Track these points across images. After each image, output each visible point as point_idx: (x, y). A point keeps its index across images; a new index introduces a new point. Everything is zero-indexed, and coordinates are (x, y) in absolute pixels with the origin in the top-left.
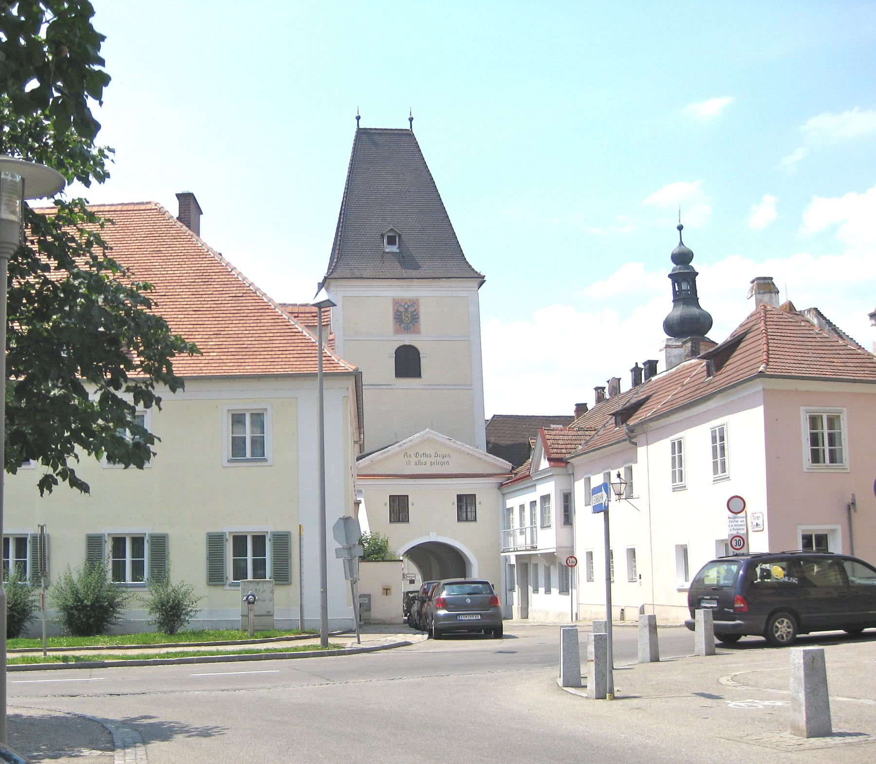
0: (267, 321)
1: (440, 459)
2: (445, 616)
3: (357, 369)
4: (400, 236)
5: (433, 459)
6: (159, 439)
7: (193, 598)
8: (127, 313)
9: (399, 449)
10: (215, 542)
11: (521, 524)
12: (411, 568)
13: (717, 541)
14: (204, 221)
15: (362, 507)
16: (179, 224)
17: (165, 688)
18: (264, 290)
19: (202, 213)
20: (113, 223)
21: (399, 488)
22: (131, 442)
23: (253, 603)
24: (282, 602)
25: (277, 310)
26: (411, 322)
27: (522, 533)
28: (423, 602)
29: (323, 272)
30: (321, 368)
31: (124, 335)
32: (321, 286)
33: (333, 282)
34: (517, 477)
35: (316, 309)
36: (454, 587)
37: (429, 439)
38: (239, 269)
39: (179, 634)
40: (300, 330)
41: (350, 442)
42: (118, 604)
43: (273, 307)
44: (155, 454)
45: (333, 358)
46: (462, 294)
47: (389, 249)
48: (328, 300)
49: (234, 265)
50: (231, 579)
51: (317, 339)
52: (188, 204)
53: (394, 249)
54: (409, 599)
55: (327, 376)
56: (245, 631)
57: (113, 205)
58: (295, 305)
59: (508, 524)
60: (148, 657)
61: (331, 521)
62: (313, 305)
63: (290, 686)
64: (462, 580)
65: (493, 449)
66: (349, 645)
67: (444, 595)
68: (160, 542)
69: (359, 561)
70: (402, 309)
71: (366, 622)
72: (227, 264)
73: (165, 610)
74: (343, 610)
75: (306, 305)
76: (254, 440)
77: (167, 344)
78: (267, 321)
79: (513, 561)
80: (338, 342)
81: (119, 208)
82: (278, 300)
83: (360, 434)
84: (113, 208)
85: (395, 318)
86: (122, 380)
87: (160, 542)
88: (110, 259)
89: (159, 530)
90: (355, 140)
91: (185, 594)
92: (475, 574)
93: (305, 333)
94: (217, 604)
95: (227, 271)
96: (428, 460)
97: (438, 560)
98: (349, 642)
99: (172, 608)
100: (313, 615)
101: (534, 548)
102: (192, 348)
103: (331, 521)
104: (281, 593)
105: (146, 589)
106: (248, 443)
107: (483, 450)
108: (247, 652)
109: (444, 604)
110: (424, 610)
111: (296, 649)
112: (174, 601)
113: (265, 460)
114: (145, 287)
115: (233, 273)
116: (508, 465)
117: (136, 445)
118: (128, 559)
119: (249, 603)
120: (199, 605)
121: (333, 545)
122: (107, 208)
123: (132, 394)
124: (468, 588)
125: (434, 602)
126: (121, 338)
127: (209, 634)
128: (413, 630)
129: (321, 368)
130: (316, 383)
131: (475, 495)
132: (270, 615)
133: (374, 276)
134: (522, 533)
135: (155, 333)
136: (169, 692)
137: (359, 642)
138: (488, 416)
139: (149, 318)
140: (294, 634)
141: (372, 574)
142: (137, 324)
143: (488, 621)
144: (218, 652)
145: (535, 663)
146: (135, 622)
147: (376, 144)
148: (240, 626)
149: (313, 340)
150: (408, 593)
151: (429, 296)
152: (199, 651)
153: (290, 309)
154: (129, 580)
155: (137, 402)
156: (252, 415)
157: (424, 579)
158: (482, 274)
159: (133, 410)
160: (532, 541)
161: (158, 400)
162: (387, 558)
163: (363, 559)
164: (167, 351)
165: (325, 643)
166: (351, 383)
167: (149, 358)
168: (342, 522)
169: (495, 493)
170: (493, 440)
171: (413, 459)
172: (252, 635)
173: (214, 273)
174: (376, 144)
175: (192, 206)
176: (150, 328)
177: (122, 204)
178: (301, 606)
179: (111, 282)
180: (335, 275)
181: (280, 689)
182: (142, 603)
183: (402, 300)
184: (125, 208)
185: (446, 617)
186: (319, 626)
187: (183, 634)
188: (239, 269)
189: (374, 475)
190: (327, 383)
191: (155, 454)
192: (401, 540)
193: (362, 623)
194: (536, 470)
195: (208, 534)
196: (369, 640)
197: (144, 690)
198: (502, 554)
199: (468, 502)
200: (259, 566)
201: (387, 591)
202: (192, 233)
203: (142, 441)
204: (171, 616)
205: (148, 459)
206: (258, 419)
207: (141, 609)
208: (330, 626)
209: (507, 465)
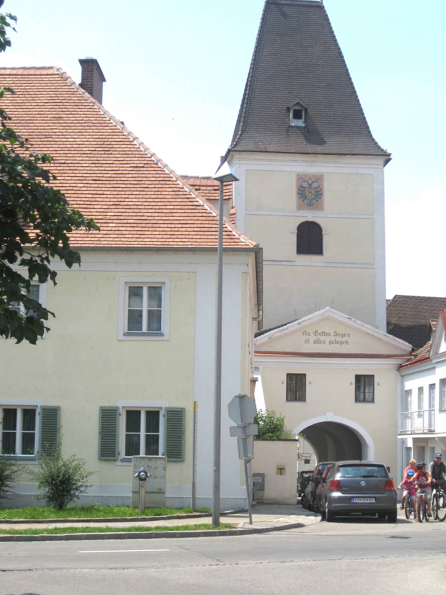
0: (168, 192)
1: (339, 339)
2: (340, 498)
3: (257, 246)
4: (306, 110)
5: (332, 338)
6: (53, 314)
7: (84, 473)
8: (25, 186)
9: (298, 327)
10: (108, 416)
11: (420, 407)
12: (306, 447)
13: (357, 400)
14: (107, 88)
15: (259, 385)
16: (82, 90)
17: (52, 565)
18: (165, 161)
19: (104, 80)
20: (13, 93)
21: (297, 366)
22: (25, 316)
23: (145, 479)
24: (175, 480)
25: (178, 182)
26: (314, 198)
27: (420, 416)
28: (317, 483)
29: (226, 142)
30: (221, 242)
31: (21, 207)
32: (224, 159)
33: (237, 156)
34: (417, 358)
35: (217, 183)
36: (349, 469)
37: (328, 318)
38: (141, 139)
39: (69, 509)
40: (201, 203)
41: (248, 319)
42: (8, 477)
43: (174, 179)
44: (48, 329)
45: (234, 233)
46: (367, 171)
47: (295, 123)
48: (231, 175)
49: (136, 134)
50: (123, 455)
51: (218, 212)
52: (92, 72)
53: (300, 123)
54: (304, 480)
55: (226, 251)
56: (136, 507)
57: (14, 69)
58: (197, 178)
59: (405, 406)
60: (36, 532)
61: (227, 398)
62: (215, 179)
63: (179, 566)
64: (357, 462)
65: (394, 329)
66: (241, 525)
67: (338, 477)
68: (52, 415)
69: (254, 440)
70: (305, 185)
71: (259, 500)
72: (129, 133)
73: (55, 485)
74: (235, 488)
75: (208, 178)
76: (150, 313)
77: (64, 219)
78: (168, 192)
79: (410, 444)
80: (240, 217)
81: (20, 72)
82: (180, 172)
83: (259, 310)
84: (14, 72)
85: (298, 194)
86: (17, 254)
87: (52, 415)
88: (9, 130)
89: (51, 403)
90: (264, 11)
91: (77, 468)
92: (372, 456)
93: (206, 207)
94: (110, 482)
95: (128, 141)
96: (327, 339)
97: (334, 441)
98: (241, 522)
99: (62, 482)
100: (205, 493)
101: (431, 432)
102: (89, 223)
103: (227, 398)
104: (173, 469)
105: (36, 462)
106: (144, 317)
107: (382, 331)
108: (137, 529)
109: (338, 486)
110: (318, 491)
111: (186, 527)
112: (64, 475)
113: (162, 335)
114: (45, 159)
115: (135, 142)
116: (408, 347)
117: (30, 319)
118: (19, 431)
119: (141, 479)
120: (90, 480)
121: (227, 423)
122: (8, 72)
123: (27, 268)
124: (363, 471)
125: (329, 484)
126: (18, 210)
127: (98, 510)
128: (307, 511)
129: (221, 242)
130: (215, 258)
131: (373, 376)
132: (161, 492)
133: (278, 149)
134: (420, 416)
135: (52, 207)
136: (55, 569)
137: (251, 523)
138: (390, 296)
139: (47, 191)
140: (186, 512)
141: (267, 453)
142: (34, 197)
143: (382, 505)
144: (108, 529)
145: (428, 549)
146: (25, 496)
147: (285, 15)
148: (130, 502)
149: (214, 214)
150: (303, 472)
151: (334, 172)
152: (87, 528)
153: (191, 182)
154: (18, 453)
155: (31, 275)
156: (149, 288)
157: (320, 460)
158: (389, 152)
159: (27, 284)
160: (430, 425)
161: (54, 275)
162: (283, 437)
163: (260, 436)
164: (64, 225)
165: (216, 523)
166: (251, 259)
167: (45, 231)
168: (237, 400)
169: (393, 375)
170: (394, 321)
171: (312, 338)
172: (143, 513)
173: (115, 142)
174: (285, 15)
175: (95, 72)
176: (47, 201)
177: (24, 68)
178: (194, 484)
179: (8, 153)
180: (238, 148)
181: (170, 569)
182: (31, 477)
183: (306, 176)
184: (26, 72)
185: (340, 499)
186: (211, 505)
187: (73, 509)
188: (142, 139)
189: (264, 353)
190: (226, 258)
191: (48, 329)
192: (298, 418)
193: (255, 503)
194: (436, 353)
195: (101, 407)
196: (261, 520)
197: (30, 566)
198: (399, 437)
199: (367, 382)
200: (152, 443)
201: (281, 470)
202: (94, 100)
203: (35, 315)
204: (61, 491)
205: (42, 334)
206: (156, 292)
207: (30, 483)
208: (222, 504)
209: (407, 346)
